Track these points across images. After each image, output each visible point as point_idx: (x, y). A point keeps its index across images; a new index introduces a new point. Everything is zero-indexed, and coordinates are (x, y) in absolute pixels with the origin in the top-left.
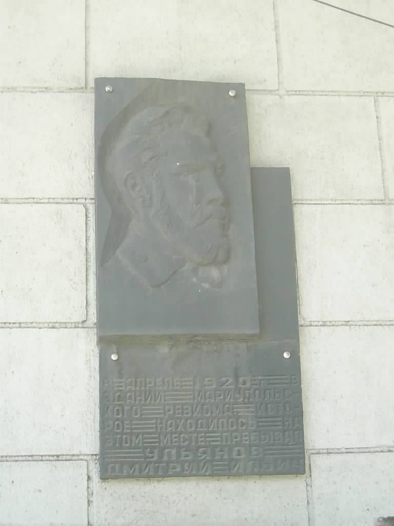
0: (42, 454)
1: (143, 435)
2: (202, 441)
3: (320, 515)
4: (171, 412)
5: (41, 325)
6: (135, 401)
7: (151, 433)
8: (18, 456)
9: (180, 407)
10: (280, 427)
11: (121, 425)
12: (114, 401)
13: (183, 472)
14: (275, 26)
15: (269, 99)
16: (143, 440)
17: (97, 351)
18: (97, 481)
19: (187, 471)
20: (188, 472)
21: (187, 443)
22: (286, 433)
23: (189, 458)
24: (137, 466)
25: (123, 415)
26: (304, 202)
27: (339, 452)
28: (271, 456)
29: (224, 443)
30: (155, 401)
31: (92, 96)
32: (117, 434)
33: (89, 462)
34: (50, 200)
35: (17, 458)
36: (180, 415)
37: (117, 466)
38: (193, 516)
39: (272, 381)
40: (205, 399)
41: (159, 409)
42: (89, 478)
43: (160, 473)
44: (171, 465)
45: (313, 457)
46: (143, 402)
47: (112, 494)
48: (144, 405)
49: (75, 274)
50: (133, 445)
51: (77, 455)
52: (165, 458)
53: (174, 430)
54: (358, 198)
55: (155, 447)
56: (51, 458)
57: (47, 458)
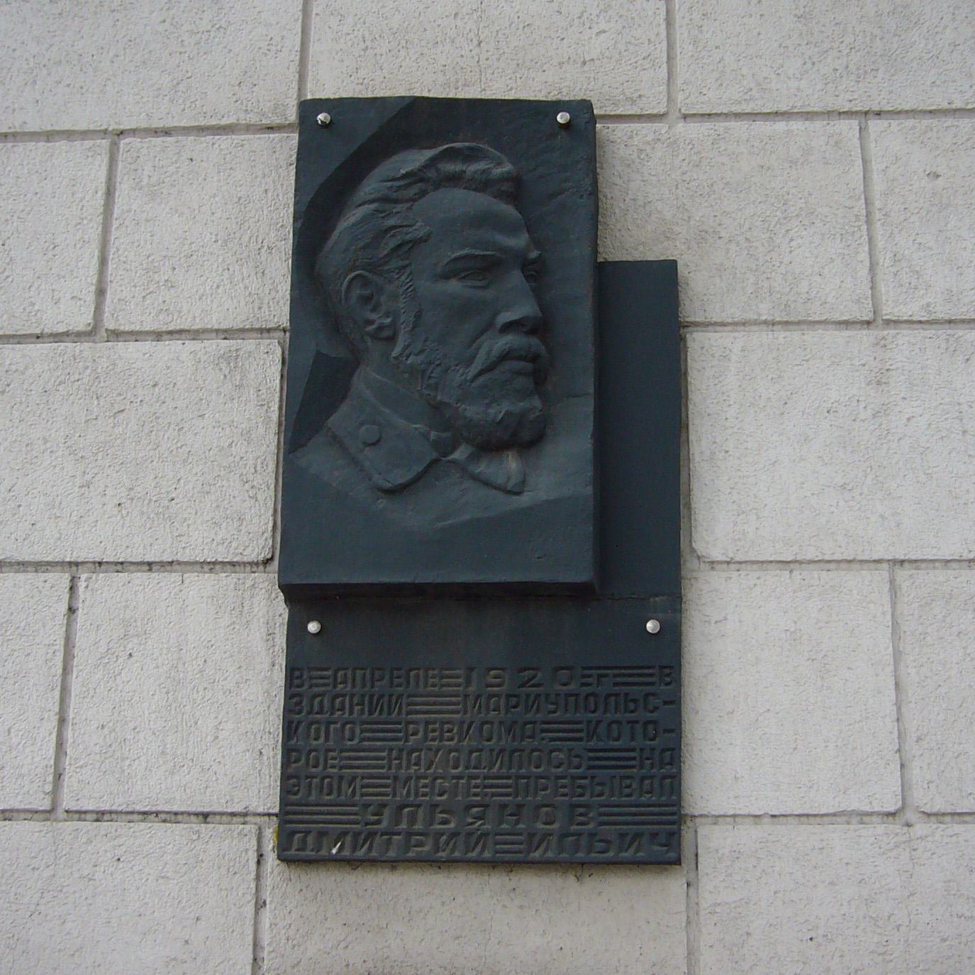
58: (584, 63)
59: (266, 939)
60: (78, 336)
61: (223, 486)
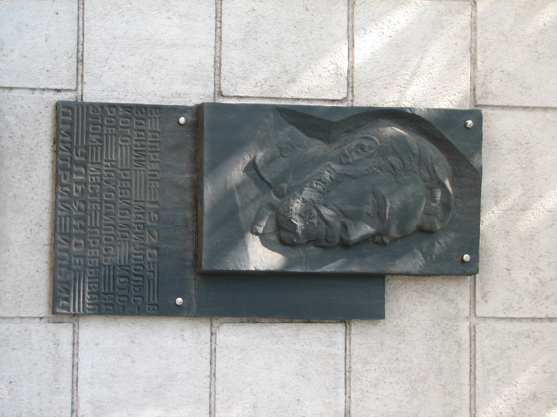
0: (85, 44)
1: (101, 146)
2: (91, 207)
4: (123, 177)
5: (218, 49)
6: (136, 140)
8: (83, 20)
9: (129, 186)
10: (103, 291)
11: (110, 124)
12: (137, 118)
13: (60, 185)
14: (552, 318)
15: (464, 304)
16: (96, 146)
17: (190, 104)
18: (55, 99)
19: (62, 190)
20: (60, 190)
22: (96, 296)
23: (75, 194)
24: (68, 139)
25: (122, 127)
27: (75, 355)
28: (72, 278)
29: (89, 230)
30: (135, 161)
32: (102, 120)
33: (74, 92)
34: (220, 14)
35: (81, 19)
36: (119, 186)
37: (69, 118)
39: (152, 284)
41: (126, 164)
42: (59, 91)
43: (60, 162)
44: (68, 174)
45: (70, 326)
46: (134, 148)
48: (131, 150)
49: (271, 86)
50: (91, 136)
51: (82, 79)
52: (75, 168)
53: (104, 178)
55: (86, 157)
56: (80, 54)
58: (508, 270)
59: (15, 93)
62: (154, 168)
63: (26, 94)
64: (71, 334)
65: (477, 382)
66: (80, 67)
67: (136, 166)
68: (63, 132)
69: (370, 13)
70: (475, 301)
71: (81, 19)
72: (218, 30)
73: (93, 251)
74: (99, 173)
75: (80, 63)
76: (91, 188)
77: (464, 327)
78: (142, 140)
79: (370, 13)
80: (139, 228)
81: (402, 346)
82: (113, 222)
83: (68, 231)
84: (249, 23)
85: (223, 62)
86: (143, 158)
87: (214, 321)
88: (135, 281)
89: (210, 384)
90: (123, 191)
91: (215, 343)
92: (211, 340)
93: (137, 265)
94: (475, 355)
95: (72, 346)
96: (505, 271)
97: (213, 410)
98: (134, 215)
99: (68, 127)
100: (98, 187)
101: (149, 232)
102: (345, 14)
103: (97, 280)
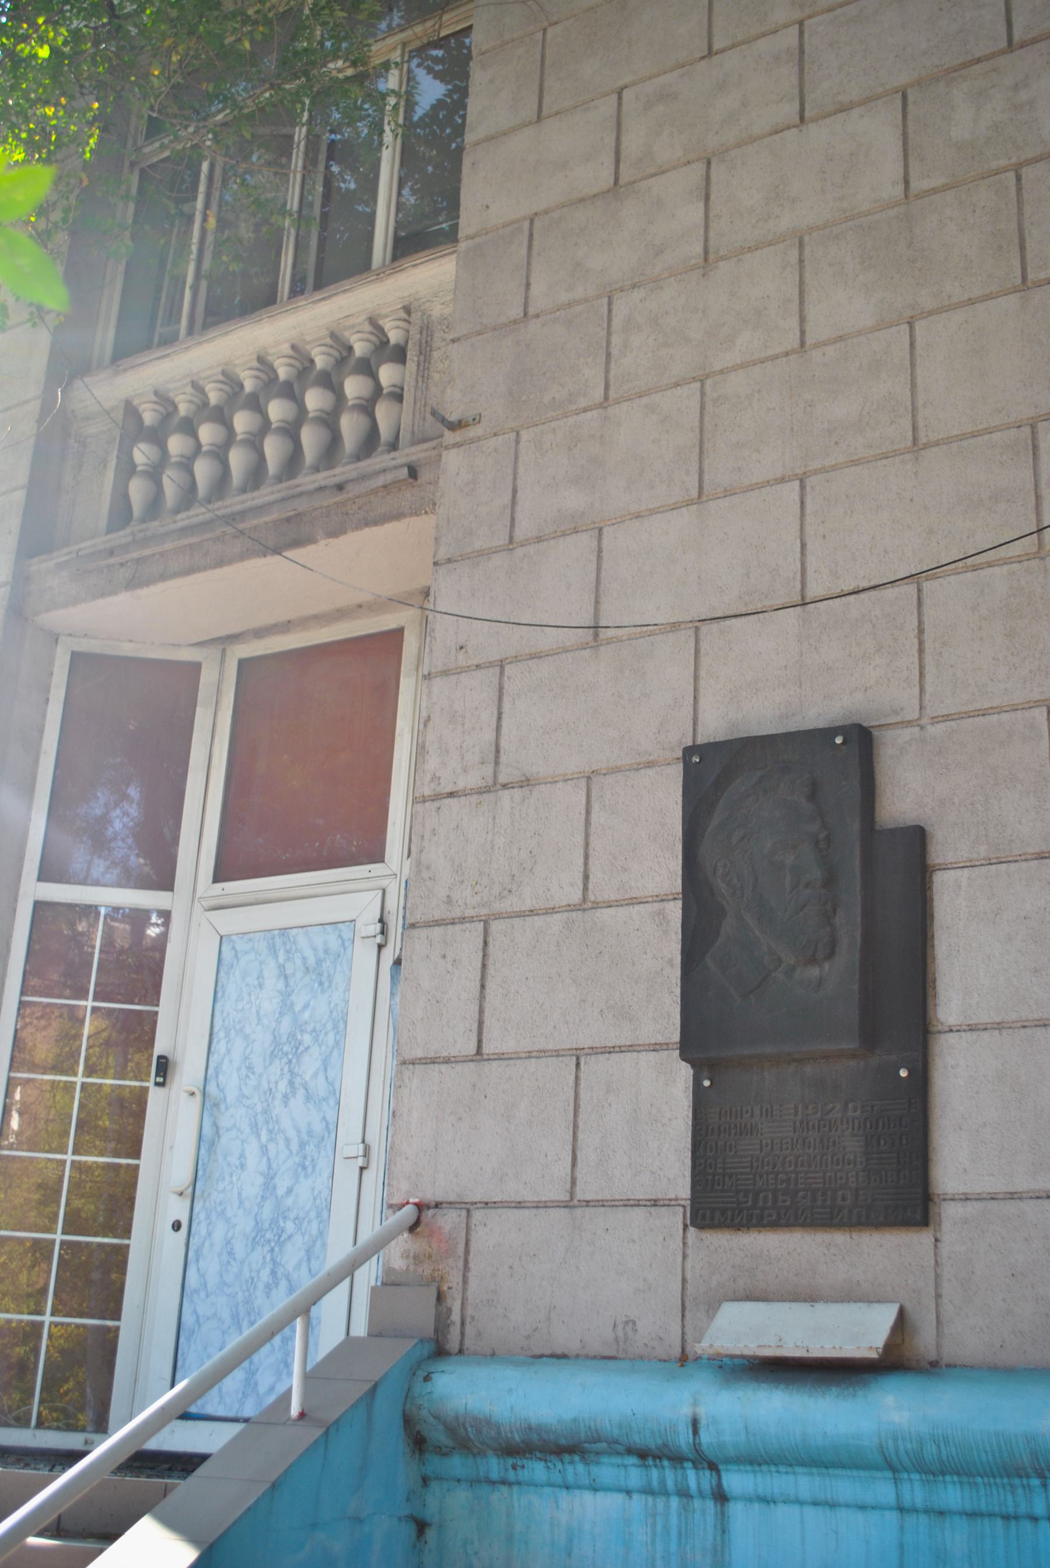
3: (950, 1280)
7: (745, 1174)
15: (905, 734)
21: (784, 1185)
23: (788, 1203)
25: (716, 1152)
26: (949, 866)
27: (979, 1198)
31: (680, 766)
35: (613, 1203)
38: (797, 1275)
40: (808, 1130)
43: (754, 1221)
47: (708, 1246)
50: (726, 1187)
52: (761, 1204)
54: (1020, 853)
57: (644, 1203)
58: (866, 690)
59: (689, 1276)
60: (594, 1051)
61: (869, 1253)
62: (759, 1112)
63: (689, 1264)
64: (952, 1203)
65: (994, 705)
66: (662, 1203)
67: (757, 1134)
68: (722, 1220)
69: (604, 884)
70: (902, 722)
71: (613, 1203)
72: (623, 1049)
73: (851, 1180)
74: (765, 1176)
75: (658, 1203)
76: (782, 1184)
77: (933, 730)
78: (730, 1128)
79: (604, 884)
80: (825, 1126)
81: (956, 800)
82: (818, 1158)
83: (828, 1210)
84: (614, 1016)
85: (653, 1041)
86: (749, 1126)
87: (935, 1029)
88: (883, 1127)
89: (1010, 1028)
90: (784, 1147)
91: (961, 1026)
92: (958, 1031)
93: (865, 1127)
94: (965, 713)
95: (969, 1202)
96: (868, 693)
97: (1041, 1023)
98: (811, 1132)
99: (717, 1214)
100: (780, 1176)
101: (827, 1114)
102: (604, 911)
103: (883, 1173)
